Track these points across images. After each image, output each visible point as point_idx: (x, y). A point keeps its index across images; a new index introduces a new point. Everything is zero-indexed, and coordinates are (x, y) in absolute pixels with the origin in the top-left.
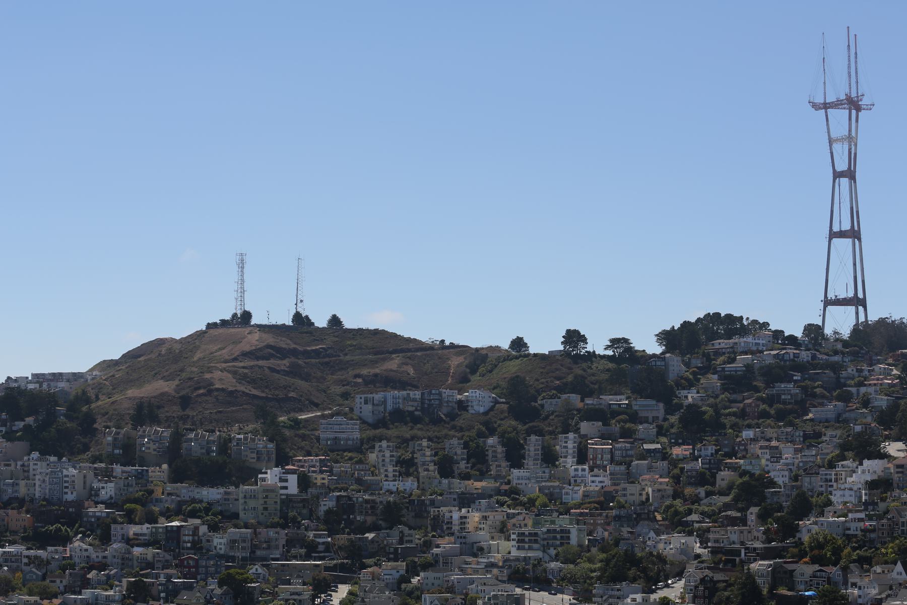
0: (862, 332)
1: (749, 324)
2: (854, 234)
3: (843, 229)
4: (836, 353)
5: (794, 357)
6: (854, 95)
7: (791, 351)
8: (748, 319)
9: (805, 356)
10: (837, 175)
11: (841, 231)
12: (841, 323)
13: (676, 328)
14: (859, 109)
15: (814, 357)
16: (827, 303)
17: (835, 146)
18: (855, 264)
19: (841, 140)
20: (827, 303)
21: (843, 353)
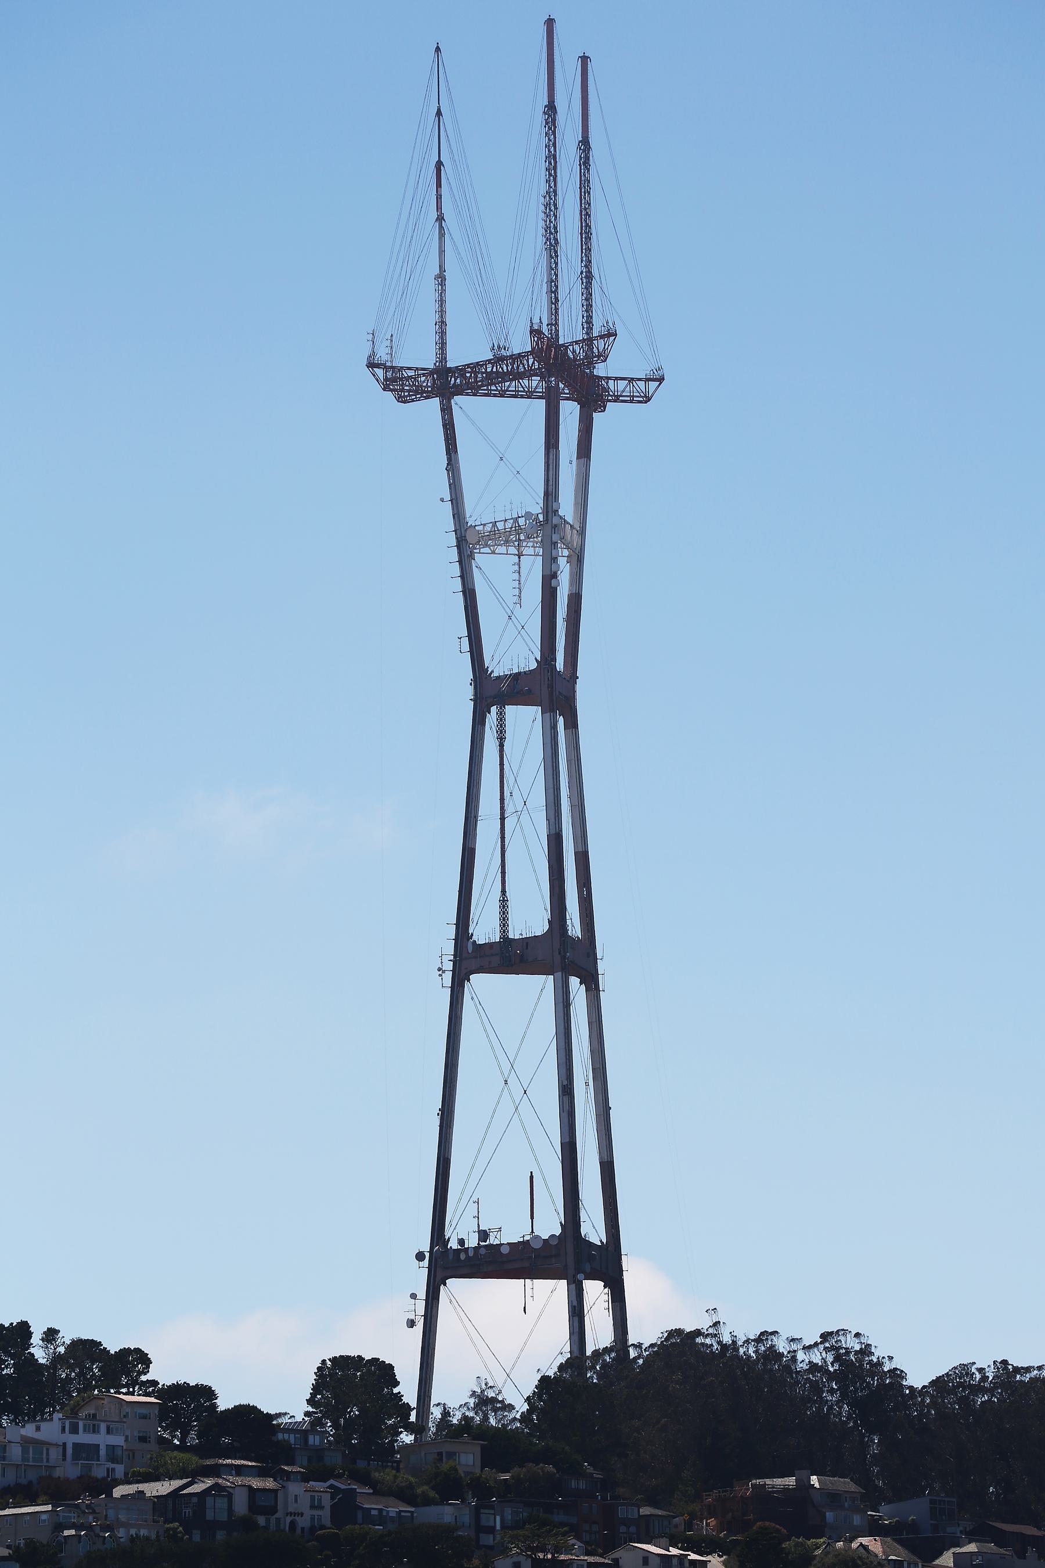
0: (584, 1394)
1: (57, 1360)
2: (565, 955)
3: (514, 934)
4: (449, 1487)
5: (254, 1507)
6: (570, 331)
7: (242, 1480)
8: (51, 1335)
9: (303, 1500)
10: (491, 693)
11: (506, 941)
12: (505, 1344)
13: (442, 1287)
14: (593, 396)
15: (345, 1507)
16: (447, 1263)
17: (482, 560)
18: (566, 1091)
19: (508, 536)
20: (447, 1263)
21: (482, 1490)
